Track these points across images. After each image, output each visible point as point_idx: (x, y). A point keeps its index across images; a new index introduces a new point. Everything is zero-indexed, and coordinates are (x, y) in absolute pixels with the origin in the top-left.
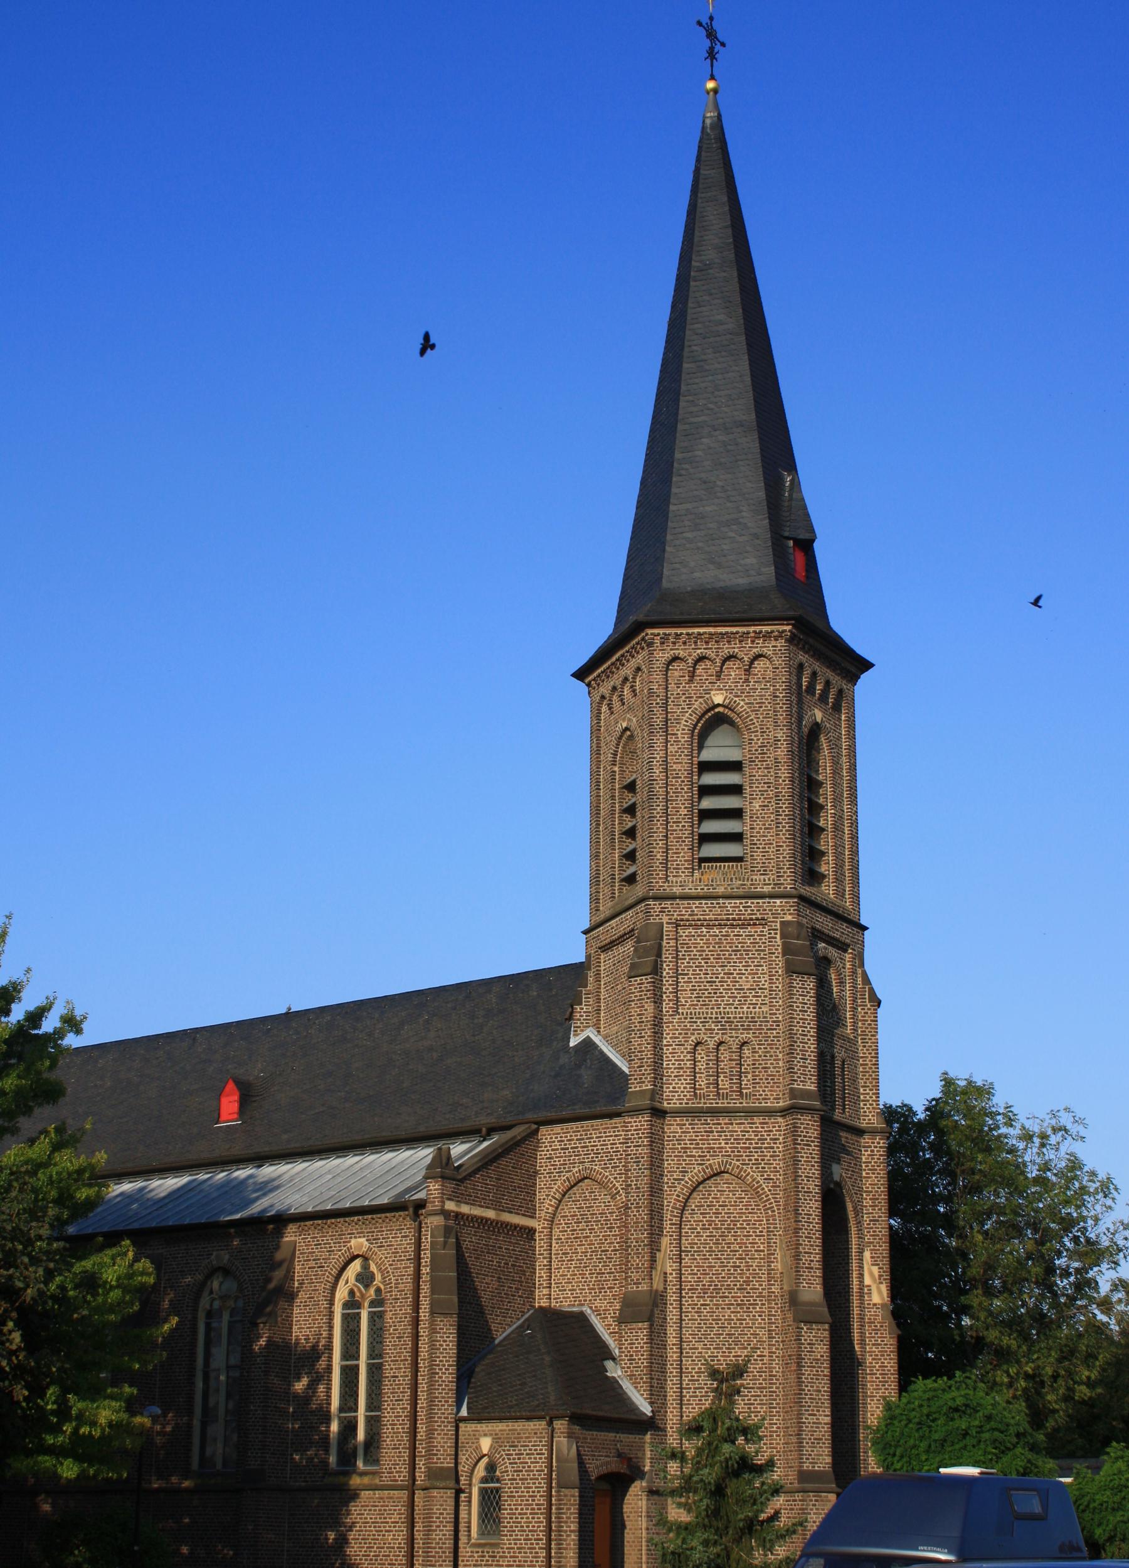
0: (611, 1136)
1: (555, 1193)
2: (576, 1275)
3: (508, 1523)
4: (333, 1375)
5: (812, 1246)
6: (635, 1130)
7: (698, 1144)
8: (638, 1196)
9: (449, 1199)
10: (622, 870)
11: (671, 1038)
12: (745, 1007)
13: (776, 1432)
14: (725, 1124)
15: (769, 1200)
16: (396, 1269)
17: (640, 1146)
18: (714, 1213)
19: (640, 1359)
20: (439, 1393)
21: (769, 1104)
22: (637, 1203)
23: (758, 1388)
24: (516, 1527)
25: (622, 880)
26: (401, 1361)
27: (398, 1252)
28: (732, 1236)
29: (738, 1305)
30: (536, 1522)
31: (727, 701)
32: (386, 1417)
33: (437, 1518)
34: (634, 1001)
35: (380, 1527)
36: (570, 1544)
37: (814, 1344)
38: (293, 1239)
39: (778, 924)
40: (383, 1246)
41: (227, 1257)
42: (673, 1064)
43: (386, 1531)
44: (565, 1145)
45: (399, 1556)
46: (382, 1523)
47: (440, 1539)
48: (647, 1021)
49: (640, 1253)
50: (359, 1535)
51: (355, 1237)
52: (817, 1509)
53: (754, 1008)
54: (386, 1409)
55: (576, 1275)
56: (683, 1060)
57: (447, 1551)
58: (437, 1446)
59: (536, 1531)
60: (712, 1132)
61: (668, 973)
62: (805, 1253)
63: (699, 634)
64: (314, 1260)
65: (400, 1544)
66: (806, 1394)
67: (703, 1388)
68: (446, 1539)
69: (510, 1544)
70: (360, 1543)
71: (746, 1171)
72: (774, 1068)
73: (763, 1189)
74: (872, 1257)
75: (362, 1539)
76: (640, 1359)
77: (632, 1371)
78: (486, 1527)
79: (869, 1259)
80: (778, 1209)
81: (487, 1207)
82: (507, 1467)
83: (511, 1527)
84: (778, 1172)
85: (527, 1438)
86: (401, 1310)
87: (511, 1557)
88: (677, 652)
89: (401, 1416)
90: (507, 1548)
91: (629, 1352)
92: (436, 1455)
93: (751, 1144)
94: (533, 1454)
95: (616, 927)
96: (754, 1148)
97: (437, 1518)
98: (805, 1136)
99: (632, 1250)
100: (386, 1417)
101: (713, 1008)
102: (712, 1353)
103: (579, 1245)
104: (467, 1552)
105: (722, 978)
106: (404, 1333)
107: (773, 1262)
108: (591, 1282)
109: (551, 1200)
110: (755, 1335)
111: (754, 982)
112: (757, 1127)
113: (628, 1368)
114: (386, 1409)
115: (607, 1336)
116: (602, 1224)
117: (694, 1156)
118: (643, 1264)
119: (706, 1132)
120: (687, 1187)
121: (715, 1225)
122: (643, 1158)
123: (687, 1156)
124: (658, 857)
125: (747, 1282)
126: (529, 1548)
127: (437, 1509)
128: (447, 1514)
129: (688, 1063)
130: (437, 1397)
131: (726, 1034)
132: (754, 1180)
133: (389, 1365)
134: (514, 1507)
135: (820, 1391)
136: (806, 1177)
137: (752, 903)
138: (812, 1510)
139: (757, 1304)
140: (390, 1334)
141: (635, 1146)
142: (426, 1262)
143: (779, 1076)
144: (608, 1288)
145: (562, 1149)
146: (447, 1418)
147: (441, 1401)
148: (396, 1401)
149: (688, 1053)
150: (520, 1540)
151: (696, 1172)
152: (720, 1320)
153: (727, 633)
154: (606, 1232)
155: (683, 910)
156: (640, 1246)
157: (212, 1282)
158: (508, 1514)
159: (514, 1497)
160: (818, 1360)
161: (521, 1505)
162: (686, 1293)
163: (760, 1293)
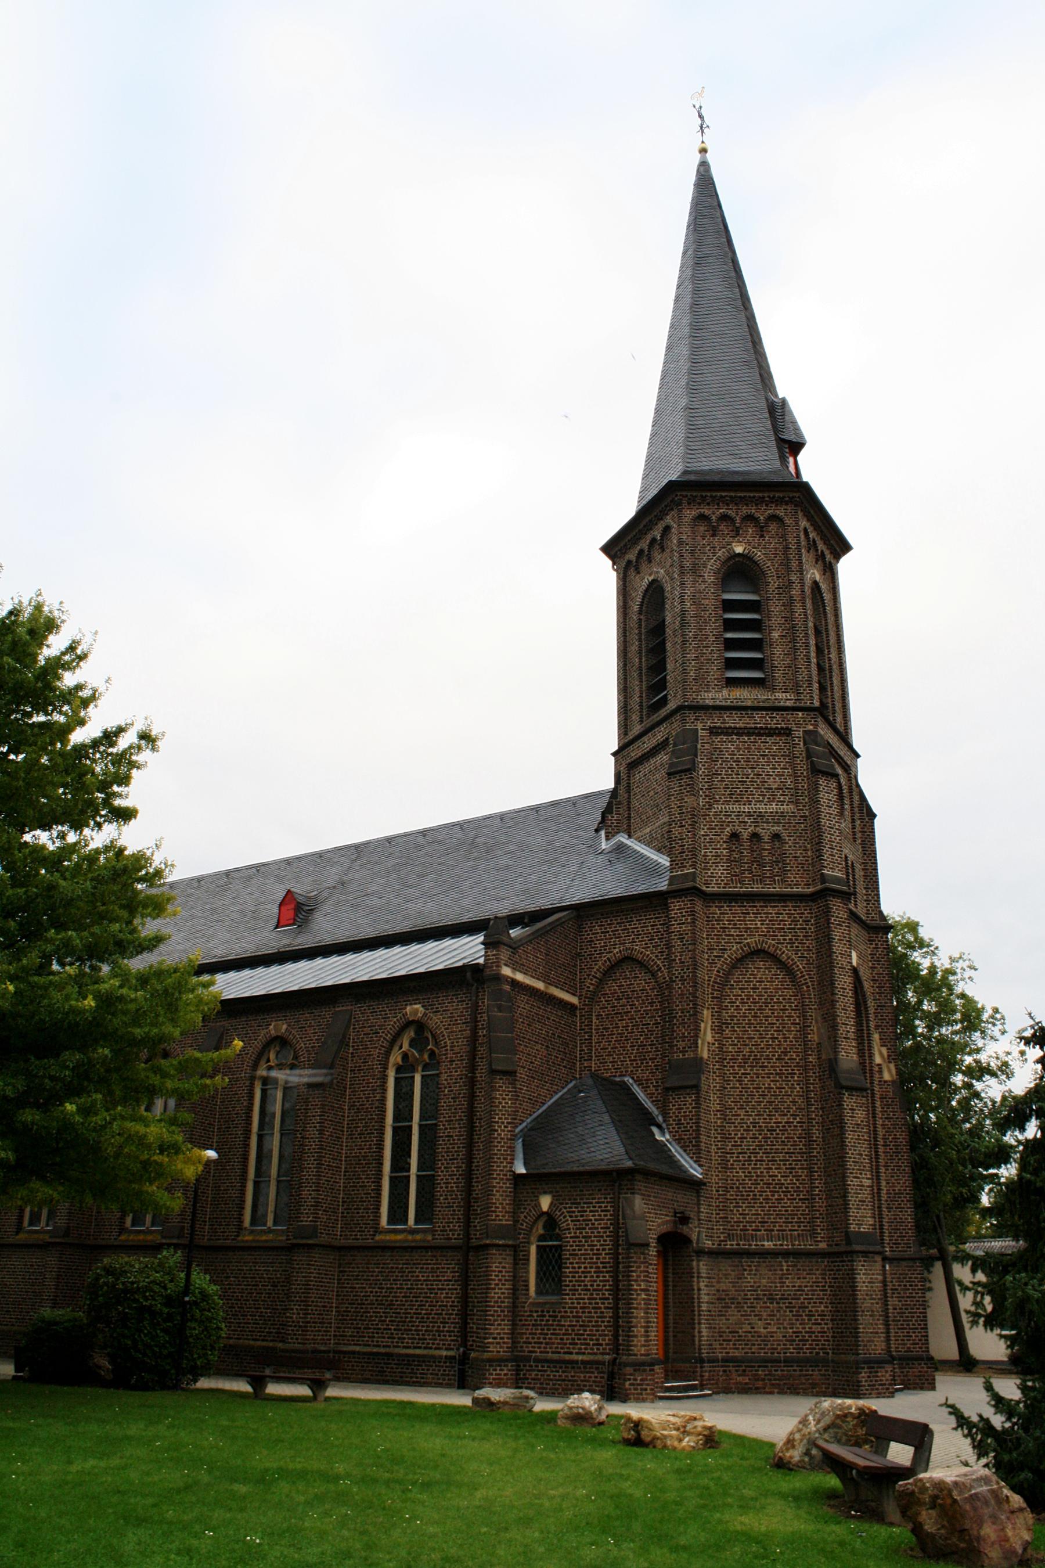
0: (652, 918)
1: (595, 973)
2: (616, 1048)
3: (570, 1281)
4: (385, 1136)
5: (847, 1017)
6: (678, 909)
7: (735, 924)
8: (682, 970)
9: (506, 965)
10: (649, 699)
11: (708, 829)
12: (774, 804)
13: (819, 1195)
14: (761, 906)
15: (804, 976)
16: (452, 1032)
17: (683, 923)
18: (752, 989)
19: (688, 1123)
20: (498, 1150)
21: (800, 890)
22: (682, 977)
23: (798, 1153)
24: (579, 1286)
25: (649, 707)
26: (456, 1120)
27: (454, 1017)
28: (770, 1010)
29: (777, 1074)
30: (601, 1281)
31: (746, 551)
32: (439, 1176)
33: (496, 1276)
34: (673, 795)
35: (432, 1285)
36: (640, 1304)
37: (855, 1110)
38: (349, 1008)
39: (801, 733)
40: (439, 1011)
41: (285, 1027)
42: (711, 852)
43: (439, 1289)
44: (606, 928)
45: (452, 1314)
46: (434, 1281)
47: (499, 1298)
48: (687, 812)
49: (686, 1023)
50: (411, 1293)
51: (411, 1004)
52: (866, 1270)
53: (782, 805)
54: (440, 1168)
55: (616, 1048)
56: (719, 849)
57: (506, 1309)
58: (495, 1203)
59: (601, 1290)
60: (749, 913)
61: (704, 772)
62: (843, 1024)
63: (721, 497)
64: (369, 1027)
65: (453, 1302)
66: (850, 1158)
67: (746, 1153)
68: (504, 1298)
69: (572, 1303)
70: (412, 1301)
71: (781, 950)
72: (804, 857)
73: (798, 966)
74: (881, 1039)
75: (413, 1297)
76: (688, 1123)
77: (680, 1135)
78: (544, 1286)
79: (878, 1041)
80: (813, 985)
81: (538, 979)
82: (568, 1225)
83: (574, 1286)
84: (811, 950)
85: (590, 1195)
86: (456, 1072)
87: (573, 1317)
88: (702, 511)
89: (456, 1175)
90: (569, 1308)
91: (677, 1116)
92: (495, 1212)
93: (785, 925)
94: (597, 1211)
95: (649, 742)
96: (788, 929)
97: (496, 1276)
98: (837, 917)
99: (678, 1020)
100: (439, 1176)
101: (744, 804)
102: (754, 1119)
103: (619, 1020)
104: (526, 1312)
105: (752, 778)
106: (460, 1094)
107: (810, 1034)
108: (632, 1053)
109: (591, 980)
110: (794, 1102)
111: (781, 782)
112: (790, 910)
113: (676, 1132)
114: (440, 1168)
115: (650, 1104)
116: (643, 1000)
117: (733, 935)
118: (689, 1033)
119: (743, 913)
120: (726, 963)
121: (754, 999)
122: (687, 934)
123: (726, 935)
124: (691, 674)
125: (785, 1053)
126: (593, 1308)
127: (496, 1267)
128: (506, 1272)
129: (724, 851)
130: (496, 1154)
131: (758, 826)
132: (789, 958)
133: (444, 1125)
134: (576, 1266)
135: (861, 1155)
136: (840, 953)
137: (777, 714)
138: (861, 1270)
139: (795, 1074)
140: (445, 1095)
141: (679, 924)
142: (483, 1025)
143: (809, 864)
144: (650, 1059)
145: (602, 933)
146: (506, 1175)
147: (500, 1158)
148: (450, 1160)
149: (724, 842)
150: (584, 1299)
151: (734, 950)
152: (760, 1088)
153: (745, 496)
154: (646, 1007)
155: (716, 720)
156: (685, 1016)
157: (269, 1051)
158: (570, 1272)
159: (577, 1255)
160: (858, 1125)
161: (584, 1263)
162: (728, 1063)
163: (798, 1063)
